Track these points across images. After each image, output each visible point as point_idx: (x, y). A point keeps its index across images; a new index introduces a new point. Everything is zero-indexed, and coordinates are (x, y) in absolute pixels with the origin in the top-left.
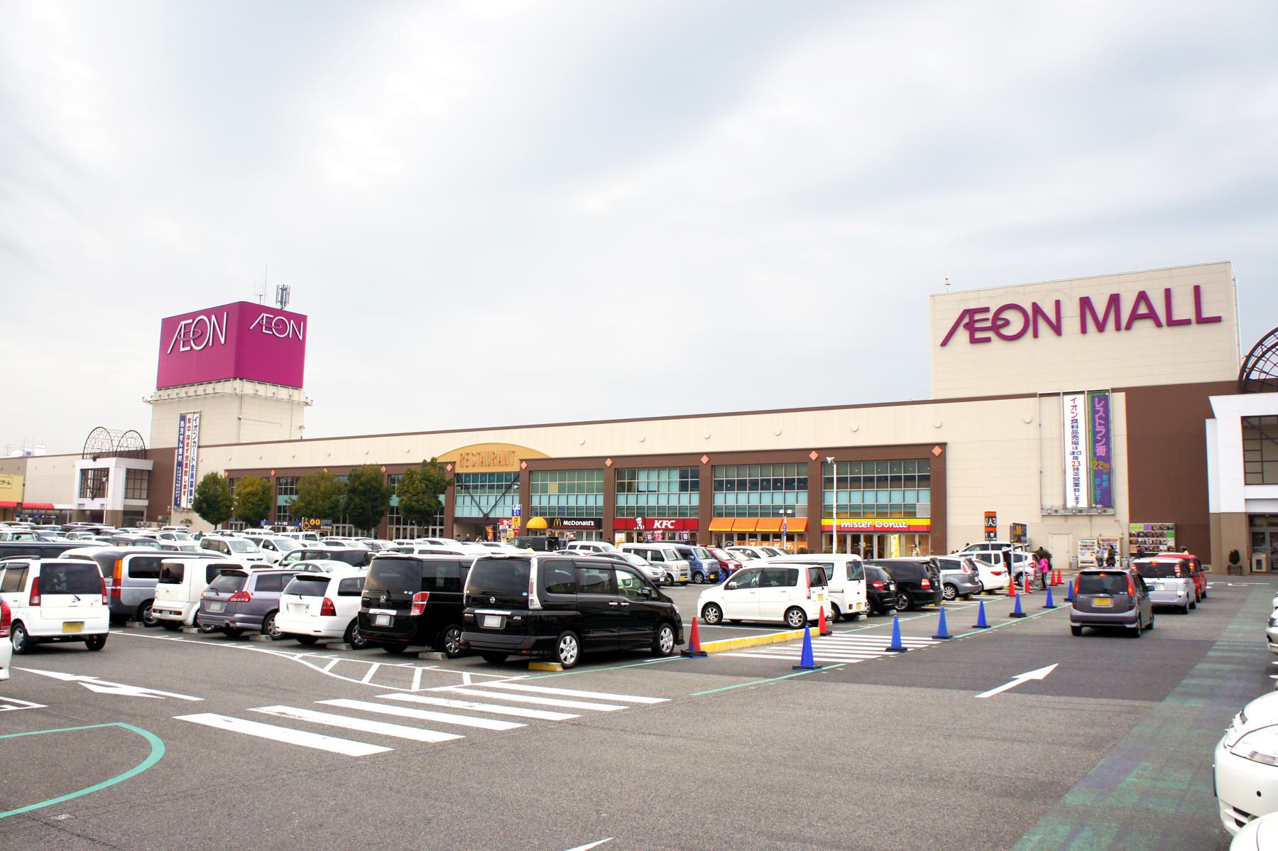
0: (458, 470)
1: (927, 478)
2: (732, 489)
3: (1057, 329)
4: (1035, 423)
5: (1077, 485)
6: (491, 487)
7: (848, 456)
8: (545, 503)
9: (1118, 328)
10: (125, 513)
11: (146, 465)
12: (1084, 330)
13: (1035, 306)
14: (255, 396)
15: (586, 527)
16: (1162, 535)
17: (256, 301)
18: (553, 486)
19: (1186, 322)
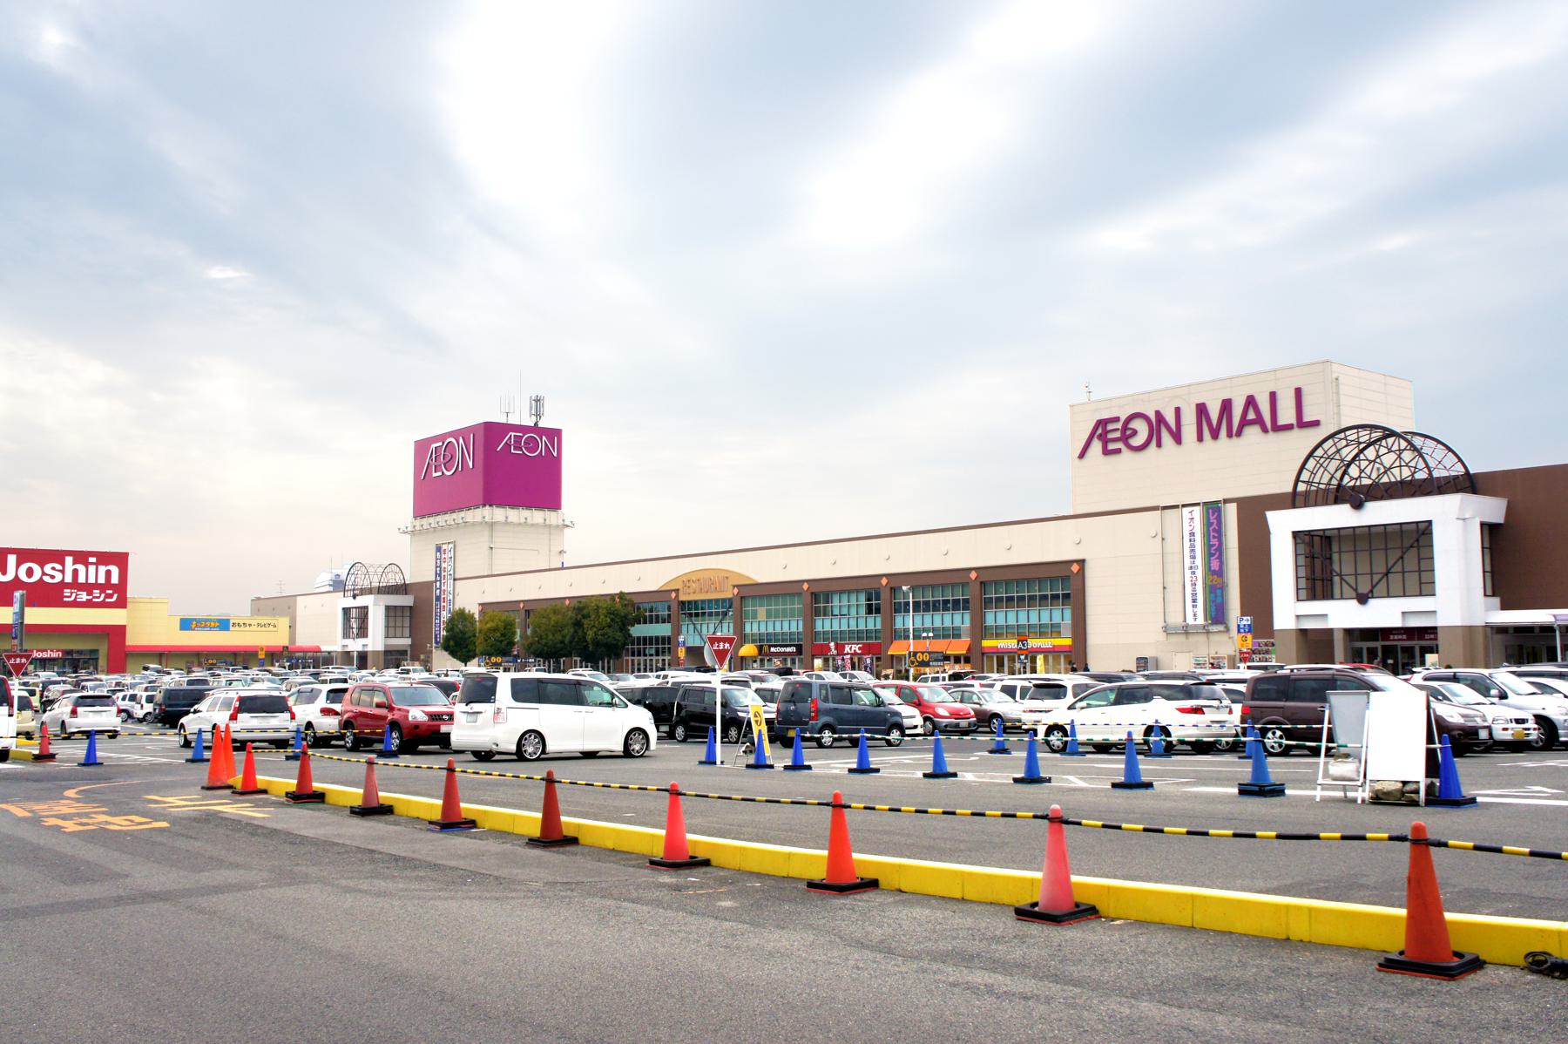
0: (682, 598)
1: (1067, 596)
2: (946, 609)
3: (1177, 437)
4: (1159, 537)
5: (1194, 601)
6: (710, 614)
7: (922, 580)
8: (755, 630)
9: (1230, 435)
10: (386, 652)
11: (406, 600)
12: (1200, 438)
13: (1158, 413)
14: (506, 523)
15: (790, 654)
16: (1267, 652)
17: (503, 420)
18: (762, 612)
19: (1289, 427)
